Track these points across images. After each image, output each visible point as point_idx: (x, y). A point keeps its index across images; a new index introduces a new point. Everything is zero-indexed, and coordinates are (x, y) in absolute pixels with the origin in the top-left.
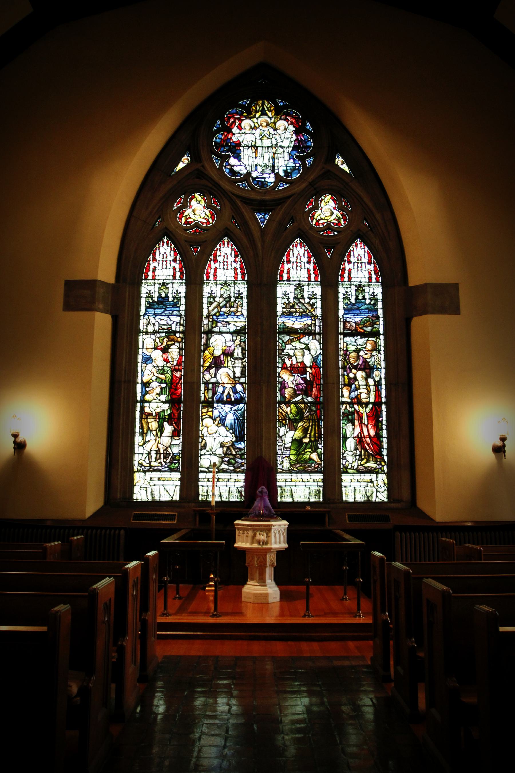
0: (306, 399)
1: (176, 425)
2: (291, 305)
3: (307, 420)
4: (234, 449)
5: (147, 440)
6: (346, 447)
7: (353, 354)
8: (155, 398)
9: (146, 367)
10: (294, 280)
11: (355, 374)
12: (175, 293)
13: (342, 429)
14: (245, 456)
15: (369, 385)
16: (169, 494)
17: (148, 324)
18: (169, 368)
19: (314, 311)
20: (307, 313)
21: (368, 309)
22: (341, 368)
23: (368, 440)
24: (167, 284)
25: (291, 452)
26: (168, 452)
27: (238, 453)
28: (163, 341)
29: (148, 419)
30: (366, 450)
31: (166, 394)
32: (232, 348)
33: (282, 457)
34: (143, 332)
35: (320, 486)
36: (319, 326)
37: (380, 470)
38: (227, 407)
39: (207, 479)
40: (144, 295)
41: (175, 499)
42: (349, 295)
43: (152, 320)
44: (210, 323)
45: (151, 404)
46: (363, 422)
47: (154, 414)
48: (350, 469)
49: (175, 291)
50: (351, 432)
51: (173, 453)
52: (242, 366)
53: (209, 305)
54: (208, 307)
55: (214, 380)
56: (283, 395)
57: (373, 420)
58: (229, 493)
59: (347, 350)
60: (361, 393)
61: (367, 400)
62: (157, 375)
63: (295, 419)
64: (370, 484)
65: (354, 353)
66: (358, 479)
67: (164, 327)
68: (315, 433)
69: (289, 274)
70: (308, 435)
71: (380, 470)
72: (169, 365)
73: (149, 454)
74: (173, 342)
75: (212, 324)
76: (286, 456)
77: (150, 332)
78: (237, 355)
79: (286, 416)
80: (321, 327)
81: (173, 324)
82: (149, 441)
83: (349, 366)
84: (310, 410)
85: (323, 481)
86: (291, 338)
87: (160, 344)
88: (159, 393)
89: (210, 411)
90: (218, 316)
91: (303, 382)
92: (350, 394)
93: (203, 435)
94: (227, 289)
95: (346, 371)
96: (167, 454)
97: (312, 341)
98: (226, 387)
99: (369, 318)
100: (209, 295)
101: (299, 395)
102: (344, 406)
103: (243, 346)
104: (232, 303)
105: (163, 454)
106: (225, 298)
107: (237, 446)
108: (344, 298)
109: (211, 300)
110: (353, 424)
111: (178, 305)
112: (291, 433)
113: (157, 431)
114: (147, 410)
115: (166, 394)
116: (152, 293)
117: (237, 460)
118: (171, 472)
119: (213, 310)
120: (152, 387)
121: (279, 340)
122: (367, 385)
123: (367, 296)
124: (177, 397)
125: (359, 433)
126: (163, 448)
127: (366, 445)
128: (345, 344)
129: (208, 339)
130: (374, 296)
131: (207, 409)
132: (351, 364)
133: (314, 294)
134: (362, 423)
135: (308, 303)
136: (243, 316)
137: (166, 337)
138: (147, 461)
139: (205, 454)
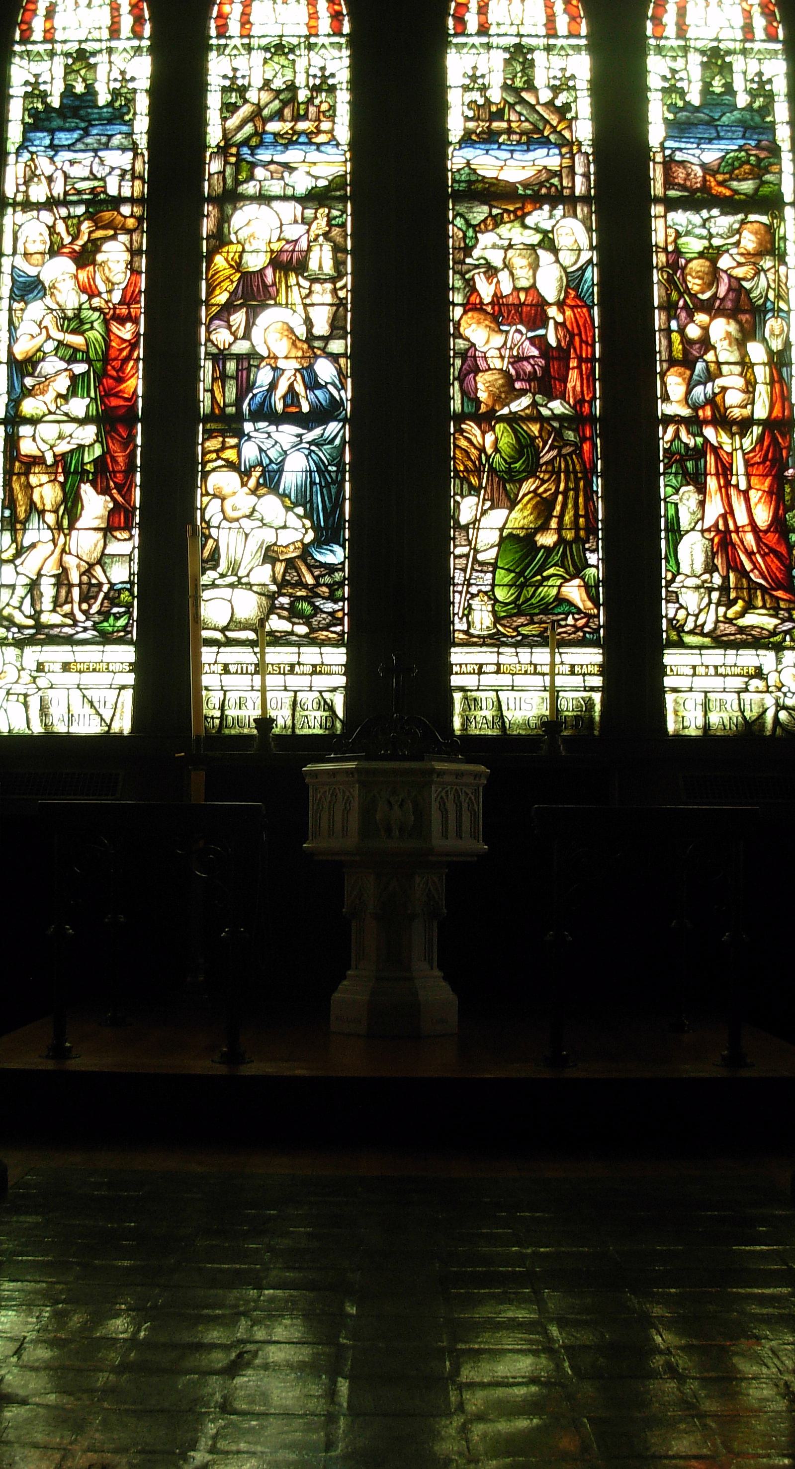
0: (546, 406)
1: (119, 492)
2: (494, 109)
3: (552, 473)
4: (310, 568)
5: (26, 543)
6: (678, 564)
7: (697, 265)
8: (53, 409)
9: (22, 310)
10: (501, 31)
11: (706, 329)
12: (115, 80)
13: (666, 503)
14: (346, 588)
15: (752, 365)
16: (101, 715)
17: (31, 179)
18: (97, 314)
19: (569, 127)
20: (546, 134)
21: (742, 123)
22: (660, 308)
23: (749, 539)
24: (94, 54)
25: (497, 576)
26: (94, 581)
27: (322, 581)
28: (79, 231)
29: (31, 476)
30: (743, 573)
31: (89, 395)
32: (303, 244)
33: (468, 592)
34: (15, 204)
35: (592, 689)
36: (586, 175)
37: (788, 638)
38: (287, 433)
39: (221, 667)
40: (17, 89)
41: (117, 730)
42: (681, 79)
43: (44, 165)
44: (229, 170)
45: (40, 427)
46: (734, 482)
47: (50, 460)
48: (692, 632)
49: (116, 74)
50: (694, 513)
51: (109, 582)
52: (336, 301)
53: (228, 115)
54: (225, 119)
55: (242, 347)
56: (470, 396)
57: (766, 476)
58: (294, 710)
59: (678, 252)
60: (724, 389)
61: (746, 412)
62: (60, 336)
63: (509, 471)
64: (755, 683)
65: (701, 261)
66: (716, 667)
67: (82, 185)
68: (577, 516)
69: (486, 14)
70: (554, 524)
71: (788, 638)
72: (96, 302)
73: (33, 586)
74: (111, 232)
75: (238, 172)
76: (480, 591)
77: (38, 203)
78: (317, 269)
79: (480, 459)
80: (592, 177)
81: (110, 173)
82: (33, 546)
83: (685, 301)
84: (560, 442)
85: (604, 670)
86: (495, 211)
87: (67, 240)
88: (64, 392)
89: (232, 447)
90: (257, 147)
91: (536, 352)
92: (688, 392)
93: (208, 523)
94: (286, 63)
95: (677, 318)
96: (90, 584)
97: (564, 222)
98: (283, 370)
99: (746, 151)
100: (227, 83)
101: (523, 393)
102: (671, 429)
103: (339, 239)
104: (302, 107)
105: (80, 585)
106: (278, 92)
107: (318, 557)
108: (664, 90)
109: (234, 98)
110: (702, 489)
111: (127, 118)
112: (497, 517)
113: (61, 513)
114: (27, 447)
115: (89, 395)
116: (45, 83)
117: (319, 602)
118: (103, 644)
119: (240, 127)
120: (44, 373)
121: (454, 217)
122: (745, 364)
123: (739, 84)
124: (122, 403)
125: (721, 515)
126: (78, 566)
127: (743, 557)
128: (671, 231)
129: (223, 220)
130: (762, 84)
131: (221, 439)
132: (693, 296)
133: (568, 75)
134: (728, 484)
135: (550, 104)
136: (338, 145)
137: (88, 215)
138: (27, 608)
139: (213, 585)
